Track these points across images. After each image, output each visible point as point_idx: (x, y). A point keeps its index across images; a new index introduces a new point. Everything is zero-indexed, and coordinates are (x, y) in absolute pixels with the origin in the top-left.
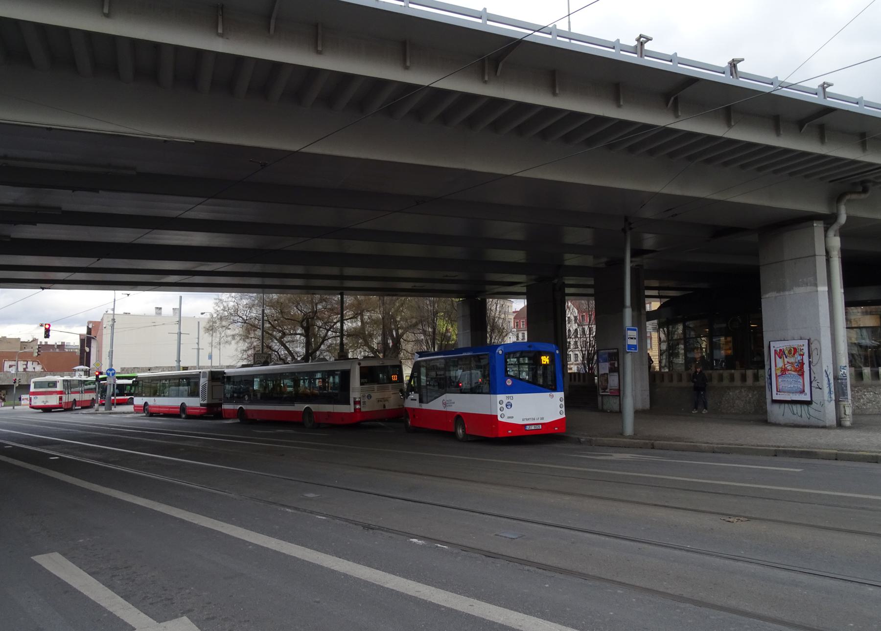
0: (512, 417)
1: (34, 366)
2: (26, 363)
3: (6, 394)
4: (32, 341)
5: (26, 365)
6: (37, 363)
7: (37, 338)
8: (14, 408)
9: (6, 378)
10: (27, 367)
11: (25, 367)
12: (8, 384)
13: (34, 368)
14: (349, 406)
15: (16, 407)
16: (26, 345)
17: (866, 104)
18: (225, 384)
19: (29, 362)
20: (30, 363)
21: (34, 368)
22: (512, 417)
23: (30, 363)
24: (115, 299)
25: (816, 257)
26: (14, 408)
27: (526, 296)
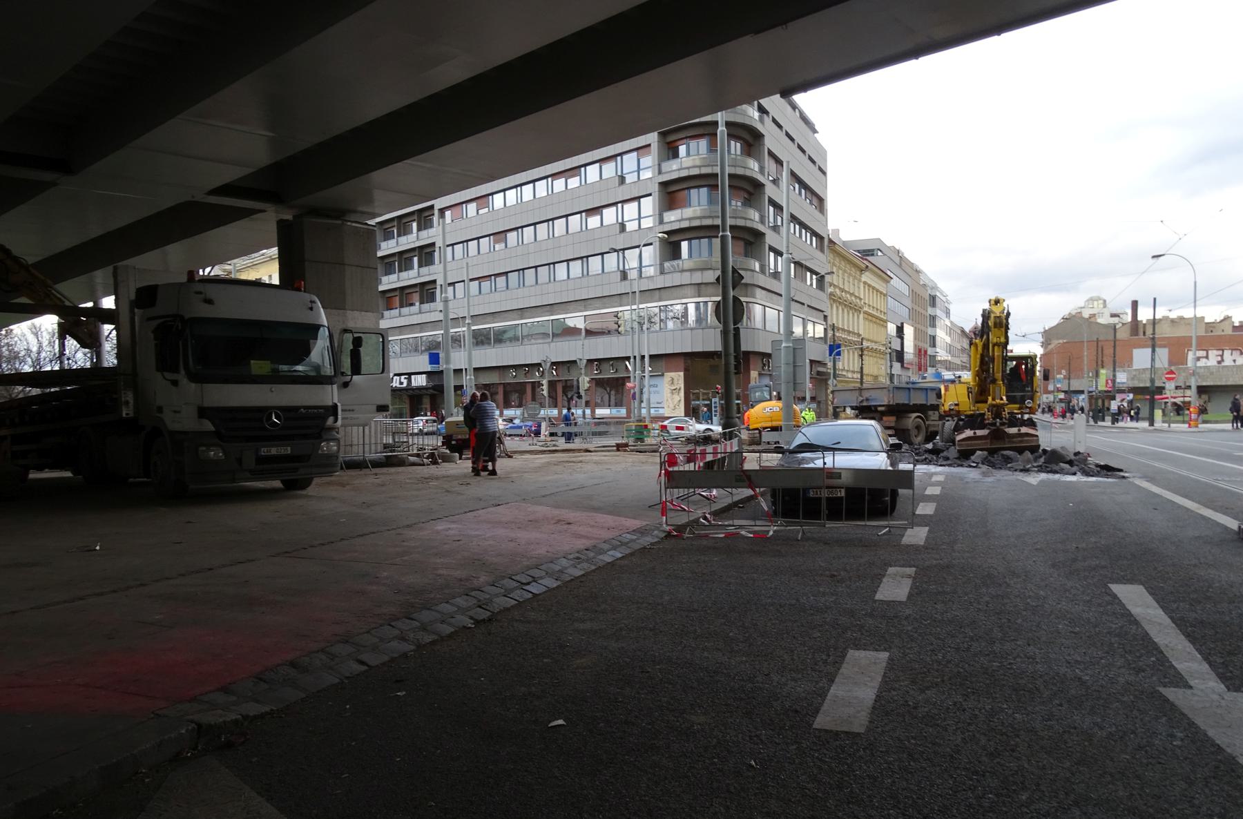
0: (839, 443)
1: (1233, 358)
2: (1220, 352)
3: (1209, 402)
4: (1222, 321)
5: (1222, 356)
6: (1238, 352)
7: (1230, 316)
8: (1169, 426)
9: (1208, 374)
10: (1223, 360)
11: (1219, 359)
12: (1212, 384)
13: (1234, 361)
14: (660, 181)
15: (1172, 425)
16: (1214, 327)
17: (779, 297)
18: (887, 452)
19: (1225, 351)
20: (1227, 353)
21: (1234, 361)
22: (839, 443)
23: (1227, 353)
24: (1195, 283)
25: (1198, 316)
26: (1169, 426)
27: (311, 341)
